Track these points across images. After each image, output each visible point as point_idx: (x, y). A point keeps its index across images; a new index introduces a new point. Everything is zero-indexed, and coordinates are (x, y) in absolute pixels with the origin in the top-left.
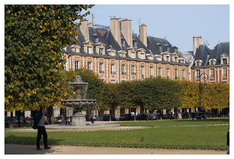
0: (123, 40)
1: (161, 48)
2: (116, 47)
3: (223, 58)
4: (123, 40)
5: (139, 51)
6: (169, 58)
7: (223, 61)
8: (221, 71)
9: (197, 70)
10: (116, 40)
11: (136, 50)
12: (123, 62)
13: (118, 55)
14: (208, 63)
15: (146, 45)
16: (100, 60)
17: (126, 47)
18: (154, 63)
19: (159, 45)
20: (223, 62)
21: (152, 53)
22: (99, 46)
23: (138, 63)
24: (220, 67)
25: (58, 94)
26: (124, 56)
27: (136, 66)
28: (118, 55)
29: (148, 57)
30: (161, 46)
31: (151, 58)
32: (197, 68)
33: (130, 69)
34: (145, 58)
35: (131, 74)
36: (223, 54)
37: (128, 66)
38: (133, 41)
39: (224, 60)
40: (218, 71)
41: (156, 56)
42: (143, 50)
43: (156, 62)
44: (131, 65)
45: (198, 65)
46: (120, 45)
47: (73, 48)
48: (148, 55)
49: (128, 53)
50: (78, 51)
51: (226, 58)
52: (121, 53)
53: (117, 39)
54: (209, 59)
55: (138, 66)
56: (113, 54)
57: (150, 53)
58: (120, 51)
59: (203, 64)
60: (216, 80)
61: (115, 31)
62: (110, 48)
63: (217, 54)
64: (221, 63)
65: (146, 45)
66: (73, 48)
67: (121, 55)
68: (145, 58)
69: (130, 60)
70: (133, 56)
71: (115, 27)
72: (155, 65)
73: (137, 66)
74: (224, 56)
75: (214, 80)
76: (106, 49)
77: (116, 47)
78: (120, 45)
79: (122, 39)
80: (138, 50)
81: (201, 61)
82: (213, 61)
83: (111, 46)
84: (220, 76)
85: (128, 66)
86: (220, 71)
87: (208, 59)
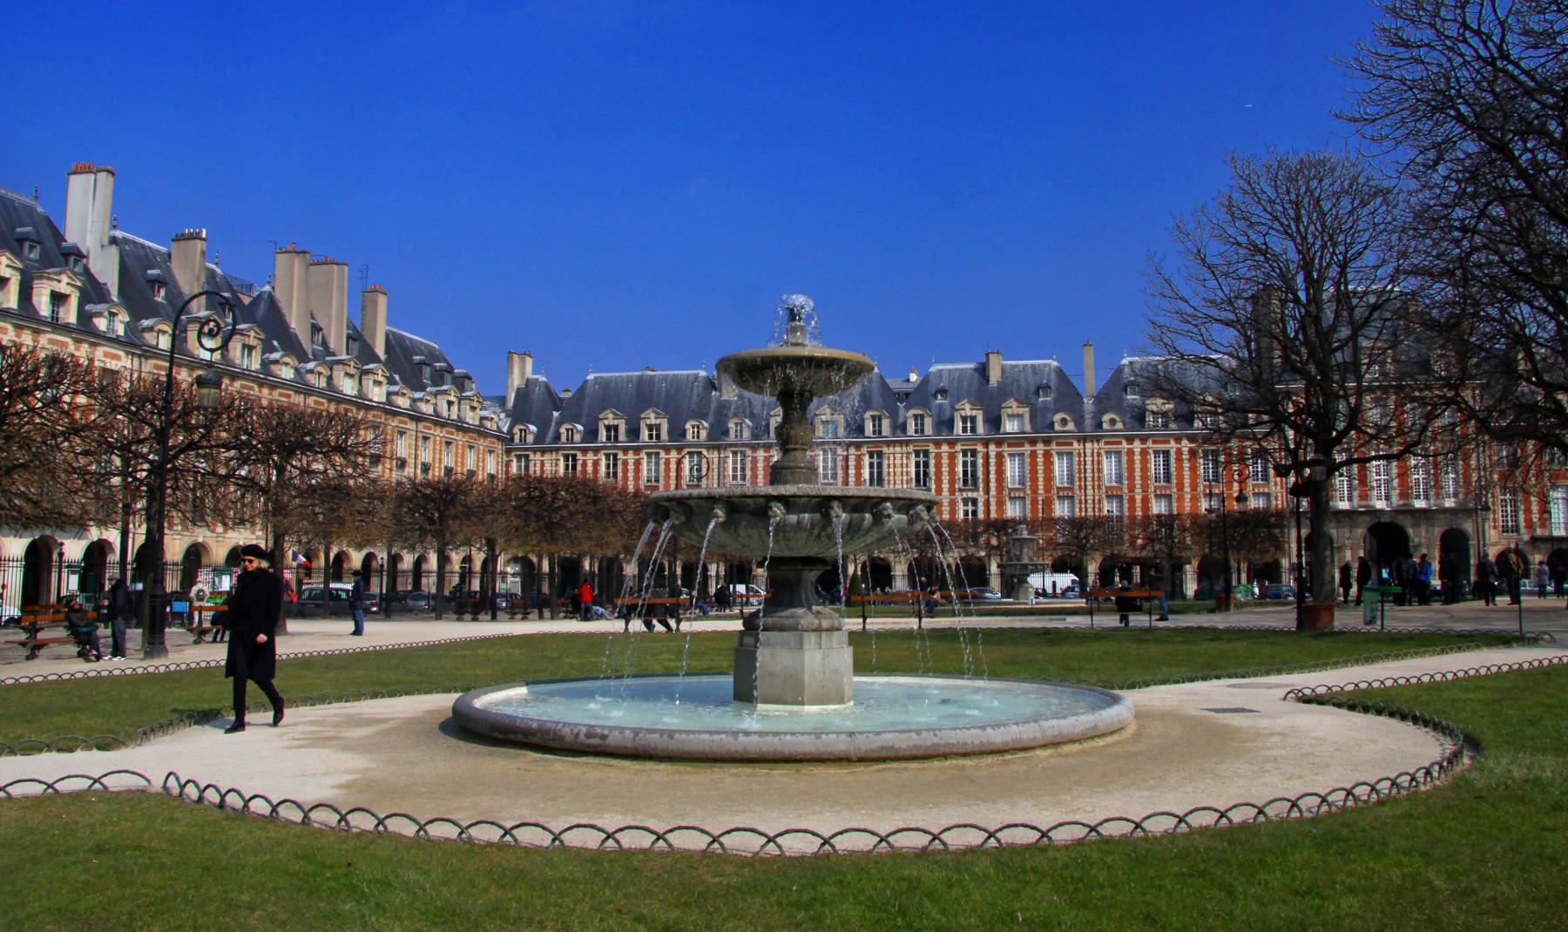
0: (316, 329)
1: (427, 371)
2: (292, 346)
4: (316, 329)
5: (368, 372)
6: (455, 408)
9: (519, 457)
14: (557, 437)
15: (382, 356)
16: (281, 395)
18: (412, 418)
19: (423, 363)
24: (596, 451)
25: (1035, 580)
26: (323, 383)
31: (403, 402)
32: (735, 445)
34: (384, 399)
38: (349, 337)
39: (608, 428)
40: (631, 462)
41: (418, 395)
43: (418, 418)
45: (523, 440)
46: (307, 345)
47: (151, 329)
49: (335, 374)
50: (164, 343)
51: (616, 422)
52: (311, 371)
53: (296, 323)
54: (560, 423)
56: (287, 373)
58: (311, 365)
59: (539, 438)
61: (291, 293)
63: (585, 411)
65: (382, 356)
66: (151, 329)
67: (312, 379)
70: (348, 387)
72: (411, 425)
77: (292, 346)
79: (313, 326)
81: (533, 428)
84: (678, 477)
86: (637, 463)
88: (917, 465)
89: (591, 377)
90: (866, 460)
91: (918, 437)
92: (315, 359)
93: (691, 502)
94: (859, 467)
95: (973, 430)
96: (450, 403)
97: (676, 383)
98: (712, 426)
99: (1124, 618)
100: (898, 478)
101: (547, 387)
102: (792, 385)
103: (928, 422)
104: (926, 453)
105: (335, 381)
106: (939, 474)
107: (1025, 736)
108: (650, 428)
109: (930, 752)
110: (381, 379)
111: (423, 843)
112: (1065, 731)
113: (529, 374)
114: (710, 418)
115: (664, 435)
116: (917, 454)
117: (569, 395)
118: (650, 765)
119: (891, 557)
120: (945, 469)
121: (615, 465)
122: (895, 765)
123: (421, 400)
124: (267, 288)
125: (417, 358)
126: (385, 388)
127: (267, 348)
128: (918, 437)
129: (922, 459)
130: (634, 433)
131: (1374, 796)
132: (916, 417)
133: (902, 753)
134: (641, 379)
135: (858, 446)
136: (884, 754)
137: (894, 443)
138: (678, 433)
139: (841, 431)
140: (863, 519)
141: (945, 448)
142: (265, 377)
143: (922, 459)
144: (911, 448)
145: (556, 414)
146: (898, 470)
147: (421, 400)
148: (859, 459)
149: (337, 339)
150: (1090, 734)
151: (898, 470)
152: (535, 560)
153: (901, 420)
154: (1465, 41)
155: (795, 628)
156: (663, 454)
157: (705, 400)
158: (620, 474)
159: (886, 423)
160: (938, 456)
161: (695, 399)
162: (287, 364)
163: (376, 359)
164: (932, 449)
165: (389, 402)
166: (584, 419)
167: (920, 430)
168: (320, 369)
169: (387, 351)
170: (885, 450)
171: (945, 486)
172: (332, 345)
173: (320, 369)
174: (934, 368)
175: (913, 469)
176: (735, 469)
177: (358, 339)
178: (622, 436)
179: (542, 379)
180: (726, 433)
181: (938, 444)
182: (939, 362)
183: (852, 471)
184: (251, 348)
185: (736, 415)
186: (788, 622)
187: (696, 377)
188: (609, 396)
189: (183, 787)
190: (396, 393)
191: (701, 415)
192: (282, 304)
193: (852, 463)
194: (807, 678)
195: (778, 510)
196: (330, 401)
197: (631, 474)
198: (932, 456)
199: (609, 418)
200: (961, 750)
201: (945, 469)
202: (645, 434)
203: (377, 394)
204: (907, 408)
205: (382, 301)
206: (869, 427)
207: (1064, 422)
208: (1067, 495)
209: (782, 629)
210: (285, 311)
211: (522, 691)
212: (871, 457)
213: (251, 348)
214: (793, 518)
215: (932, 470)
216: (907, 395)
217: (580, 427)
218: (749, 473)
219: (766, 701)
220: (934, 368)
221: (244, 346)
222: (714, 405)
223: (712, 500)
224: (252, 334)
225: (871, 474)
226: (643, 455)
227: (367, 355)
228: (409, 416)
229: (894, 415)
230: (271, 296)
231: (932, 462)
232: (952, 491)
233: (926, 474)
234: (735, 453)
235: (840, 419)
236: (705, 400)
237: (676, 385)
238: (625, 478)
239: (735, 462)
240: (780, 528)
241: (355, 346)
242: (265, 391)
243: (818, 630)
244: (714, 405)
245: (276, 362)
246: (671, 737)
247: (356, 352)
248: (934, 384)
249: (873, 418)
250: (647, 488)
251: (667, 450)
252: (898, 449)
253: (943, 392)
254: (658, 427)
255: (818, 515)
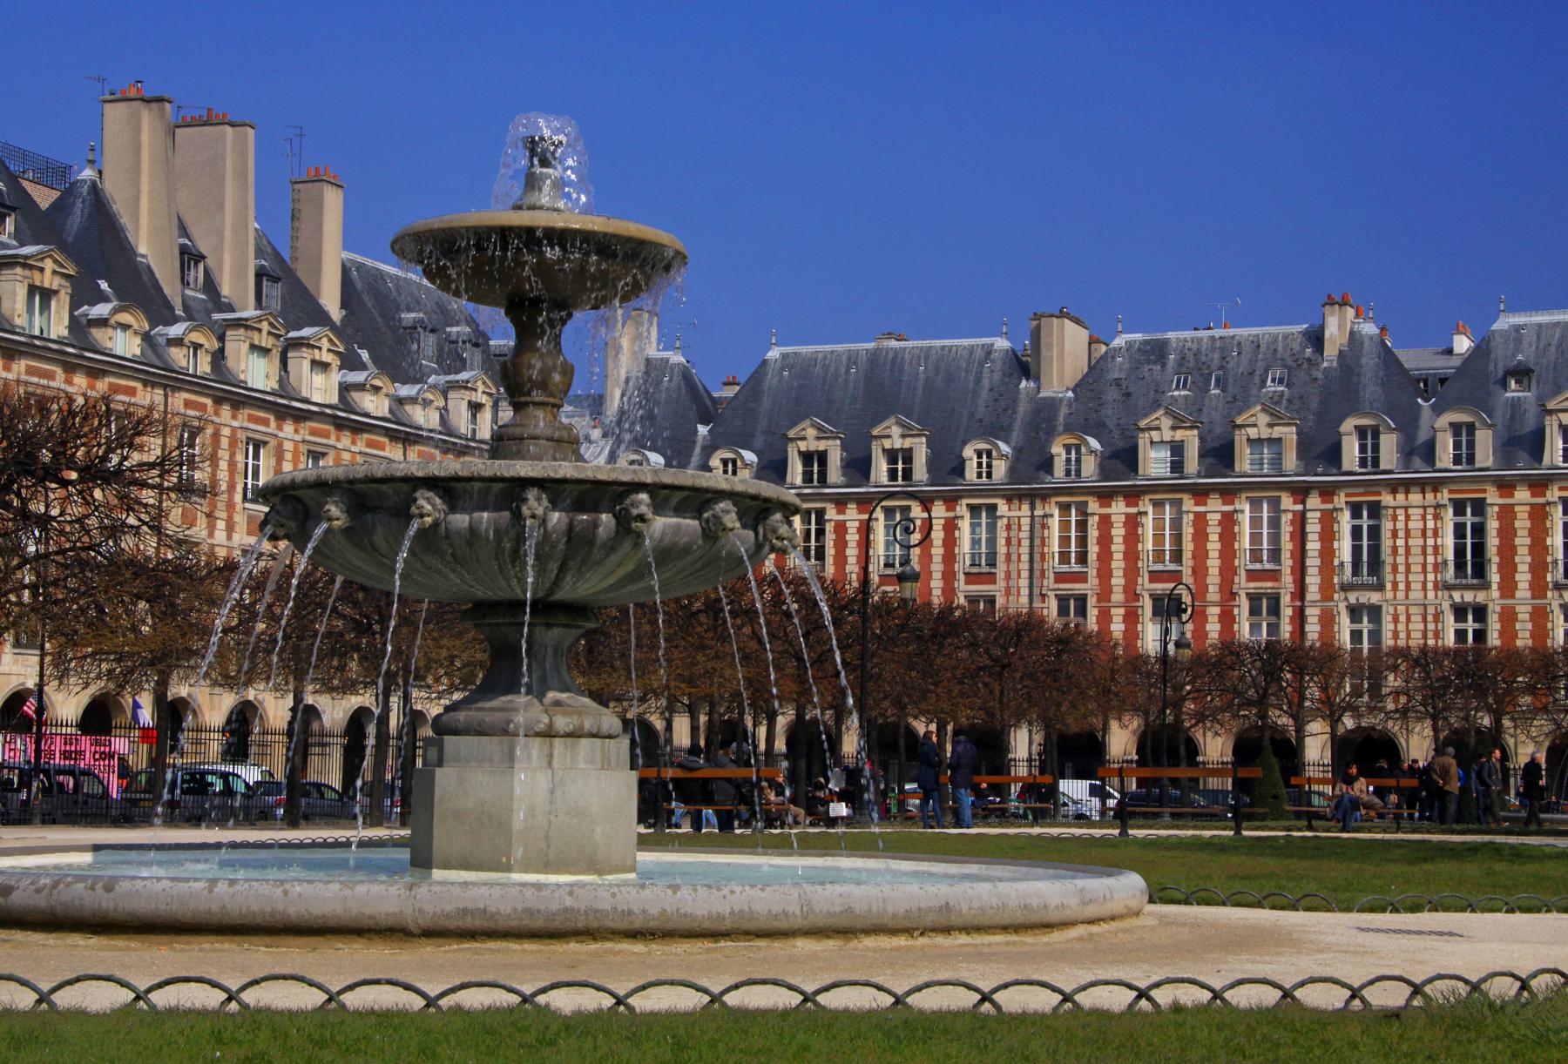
0: (190, 256)
1: (429, 342)
2: (139, 291)
3: (803, 446)
4: (190, 256)
6: (486, 416)
7: (799, 468)
8: (956, 527)
10: (142, 249)
11: (278, 337)
12: (187, 404)
13: (159, 357)
15: (336, 313)
16: (30, 371)
17: (210, 306)
18: (394, 436)
20: (804, 473)
21: (372, 368)
22: (27, 273)
23: (288, 428)
26: (204, 366)
27: (273, 442)
28: (159, 357)
29: (355, 395)
30: (433, 331)
31: (374, 405)
33: (232, 464)
34: (335, 400)
35: (238, 498)
36: (807, 423)
37: (225, 442)
38: (260, 275)
39: (807, 457)
40: (853, 527)
41: (406, 390)
42: (325, 344)
44: (242, 435)
46: (171, 288)
48: (358, 377)
49: (229, 347)
51: (907, 443)
52: (178, 342)
53: (149, 244)
54: (709, 450)
55: (288, 446)
56: (126, 345)
57: (363, 367)
58: (176, 330)
60: (1001, 582)
61: (136, 185)
62: (103, 298)
63: (763, 423)
64: (873, 478)
65: (336, 313)
67: (178, 356)
68: (335, 400)
69: (240, 399)
70: (258, 373)
71: (139, 155)
73: (280, 445)
74: (811, 432)
75: (1081, 577)
76: (74, 306)
77: (139, 291)
78: (167, 291)
79: (184, 251)
80: (293, 334)
82: (734, 462)
83: (104, 285)
85: (225, 442)
87: (704, 448)
88: (1459, 531)
89: (774, 354)
90: (1345, 521)
91: (1461, 471)
92: (190, 318)
93: (301, 493)
94: (1328, 536)
96: (475, 407)
97: (945, 366)
98: (1018, 451)
100: (1416, 559)
101: (686, 376)
102: (533, 283)
103: (1485, 441)
104: (1479, 507)
105: (230, 362)
106: (1507, 551)
107: (760, 908)
108: (892, 456)
109: (558, 924)
110: (327, 357)
112: (860, 908)
113: (653, 351)
114: (1016, 434)
115: (920, 472)
116: (1459, 508)
117: (730, 392)
118: (77, 939)
119: (1394, 727)
120: (1522, 541)
121: (821, 533)
122: (492, 945)
123: (413, 400)
124: (88, 174)
125: (409, 317)
126: (336, 377)
127: (84, 293)
128: (1461, 471)
129: (1469, 519)
130: (858, 467)
132: (1456, 428)
133: (502, 924)
134: (874, 356)
135: (1327, 492)
136: (469, 923)
137: (1407, 486)
138: (948, 467)
139: (1291, 461)
140: (595, 524)
141: (1522, 495)
142: (81, 352)
143: (1469, 519)
144: (1445, 496)
145: (703, 430)
146: (1416, 542)
147: (413, 400)
148: (1328, 520)
149: (235, 278)
150: (929, 920)
151: (1416, 542)
152: (659, 725)
153: (1422, 436)
155: (504, 731)
157: (1005, 398)
158: (830, 551)
159: (1389, 444)
160: (1507, 513)
161: (984, 394)
162: (126, 327)
163: (321, 318)
164: (1492, 497)
165: (345, 402)
166: (759, 440)
167: (1465, 455)
168: (196, 337)
169: (345, 304)
170: (1387, 499)
171: (1523, 577)
172: (226, 290)
173: (196, 337)
174: (1504, 323)
175: (1449, 541)
176: (1064, 540)
177: (282, 279)
178: (835, 474)
179: (677, 358)
180: (1047, 465)
181: (1506, 487)
182: (1513, 309)
183: (1313, 546)
184: (47, 295)
185: (1069, 429)
186: (488, 718)
187: (988, 351)
188: (809, 394)
190: (361, 387)
191: (996, 429)
192: (120, 207)
193: (1313, 528)
194: (519, 819)
195: (429, 505)
196: (218, 401)
197: (852, 552)
198: (1492, 511)
199: (809, 438)
200: (622, 925)
201: (1522, 541)
202: (880, 469)
203: (320, 388)
204: (1438, 410)
205: (333, 201)
206: (1351, 451)
209: (481, 731)
210: (125, 220)
212: (1356, 514)
213: (47, 295)
214: (461, 520)
215: (1492, 542)
216: (1443, 381)
217: (750, 456)
218: (1093, 550)
219: (447, 866)
220: (1504, 323)
221: (32, 289)
222: (1023, 408)
223: (324, 487)
224: (49, 265)
225: (1357, 551)
226: (879, 514)
227: (301, 306)
228: (388, 433)
229: (1407, 424)
230: (95, 189)
231: (1493, 525)
232: (1538, 588)
233: (1479, 549)
234: (1065, 508)
235: (1289, 434)
236: (1005, 398)
237: (946, 370)
238: (841, 559)
239: (1065, 526)
240: (430, 538)
241: (274, 292)
242: (80, 380)
243: (549, 734)
244: (1023, 408)
245: (103, 322)
246: (109, 889)
247: (276, 305)
248: (1501, 358)
249: (1361, 432)
250: (884, 579)
252: (1415, 498)
253: (1522, 374)
254: (908, 455)
255: (506, 514)
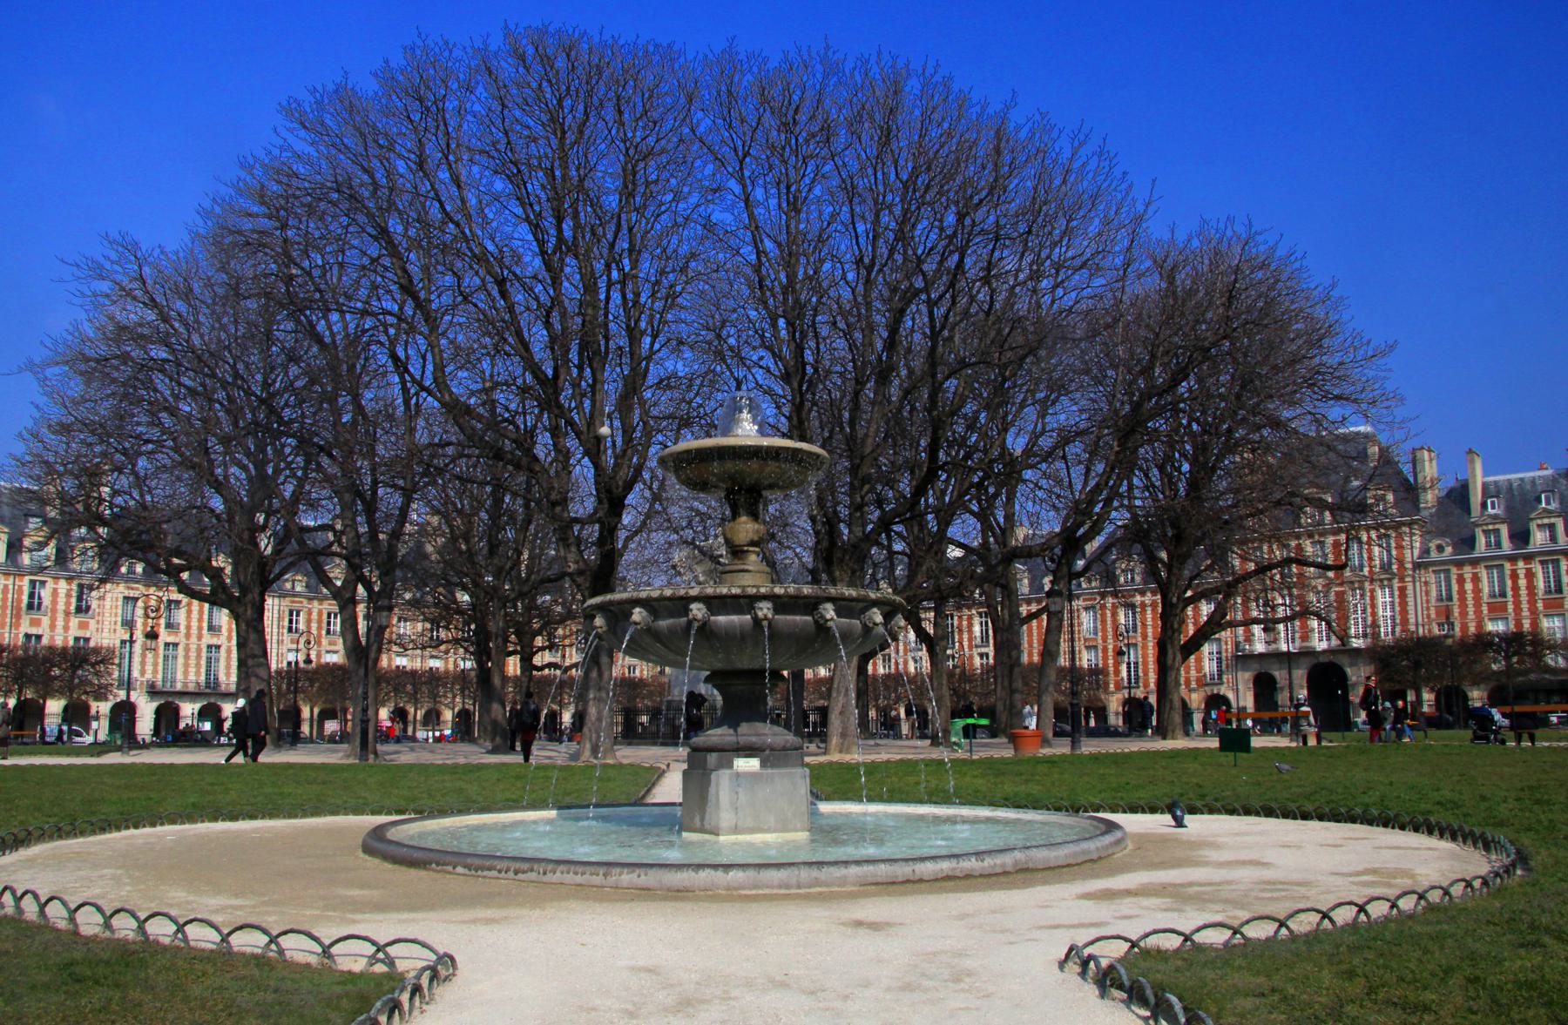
24: (1528, 558)
40: (1521, 573)
95: (1498, 545)
99: (1074, 744)
111: (224, 956)
131: (1362, 917)
141: (1521, 564)
154: (560, 238)
156: (1508, 566)
189: (42, 906)
207: (1440, 549)
208: (1497, 610)
211: (553, 813)
251: (1512, 559)
